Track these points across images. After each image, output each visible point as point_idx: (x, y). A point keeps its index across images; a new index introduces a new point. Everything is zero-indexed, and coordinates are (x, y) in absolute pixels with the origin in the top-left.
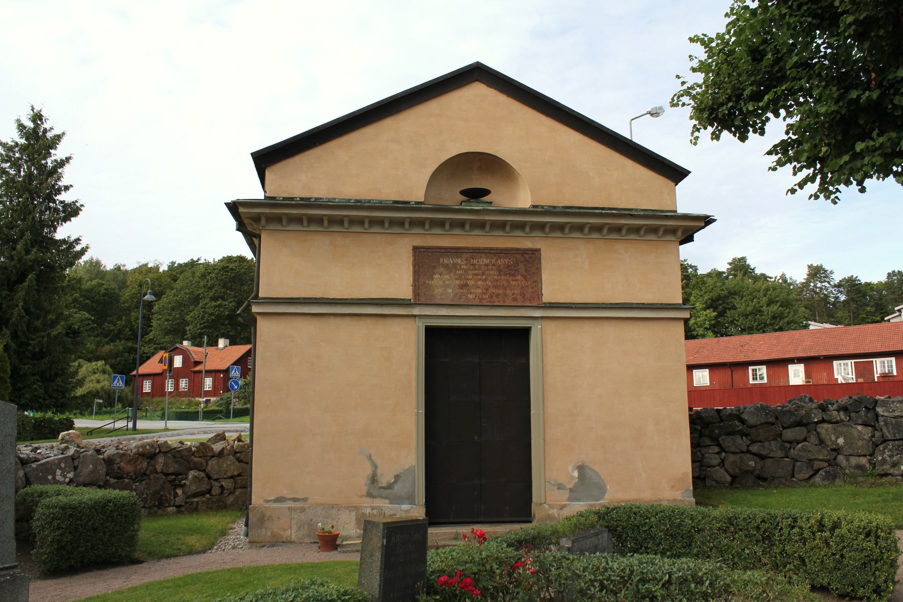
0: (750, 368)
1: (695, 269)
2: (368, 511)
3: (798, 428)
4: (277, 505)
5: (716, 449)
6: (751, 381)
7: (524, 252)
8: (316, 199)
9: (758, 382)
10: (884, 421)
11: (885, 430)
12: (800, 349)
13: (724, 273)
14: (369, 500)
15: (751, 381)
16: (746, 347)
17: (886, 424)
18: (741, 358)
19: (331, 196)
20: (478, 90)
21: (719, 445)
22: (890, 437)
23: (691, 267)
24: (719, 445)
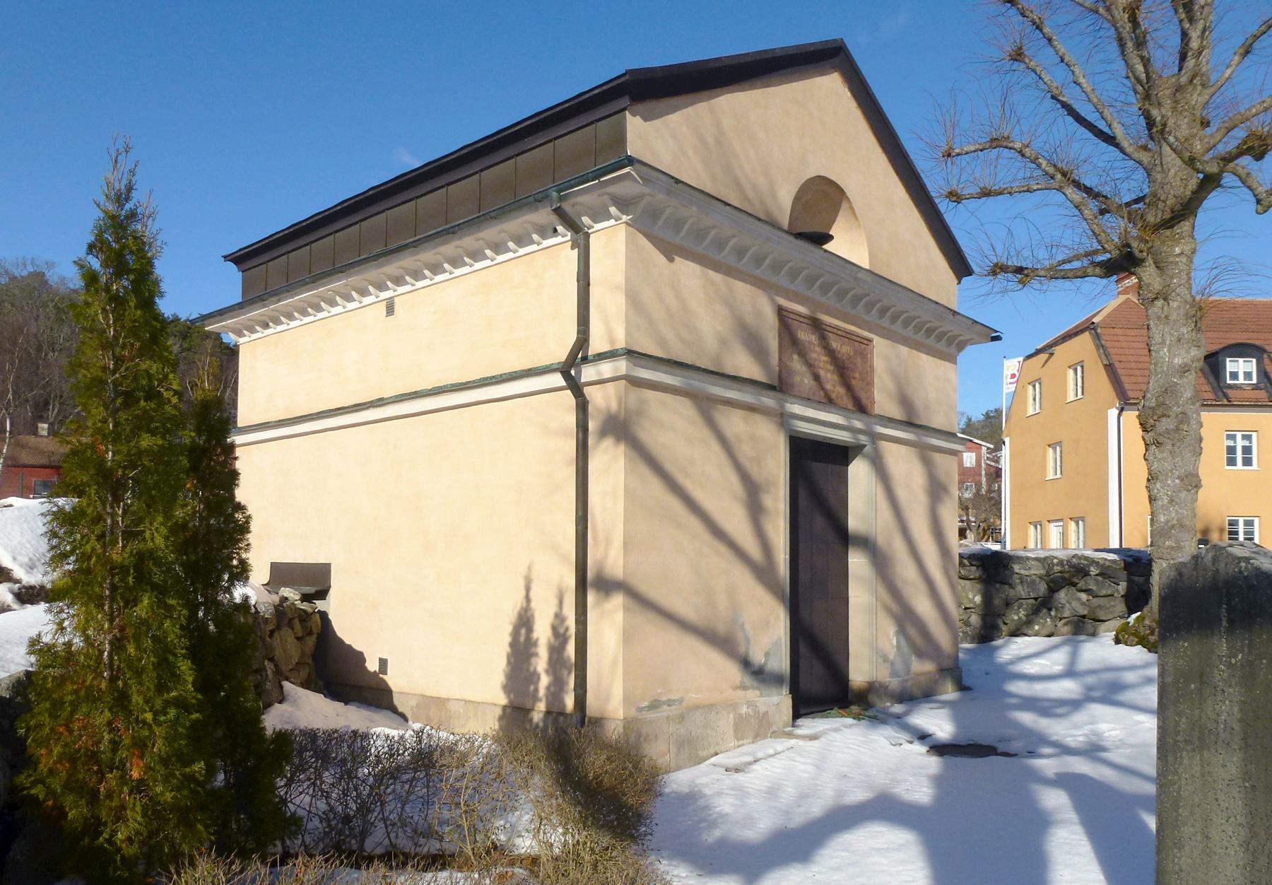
4: (652, 715)
14: (740, 693)
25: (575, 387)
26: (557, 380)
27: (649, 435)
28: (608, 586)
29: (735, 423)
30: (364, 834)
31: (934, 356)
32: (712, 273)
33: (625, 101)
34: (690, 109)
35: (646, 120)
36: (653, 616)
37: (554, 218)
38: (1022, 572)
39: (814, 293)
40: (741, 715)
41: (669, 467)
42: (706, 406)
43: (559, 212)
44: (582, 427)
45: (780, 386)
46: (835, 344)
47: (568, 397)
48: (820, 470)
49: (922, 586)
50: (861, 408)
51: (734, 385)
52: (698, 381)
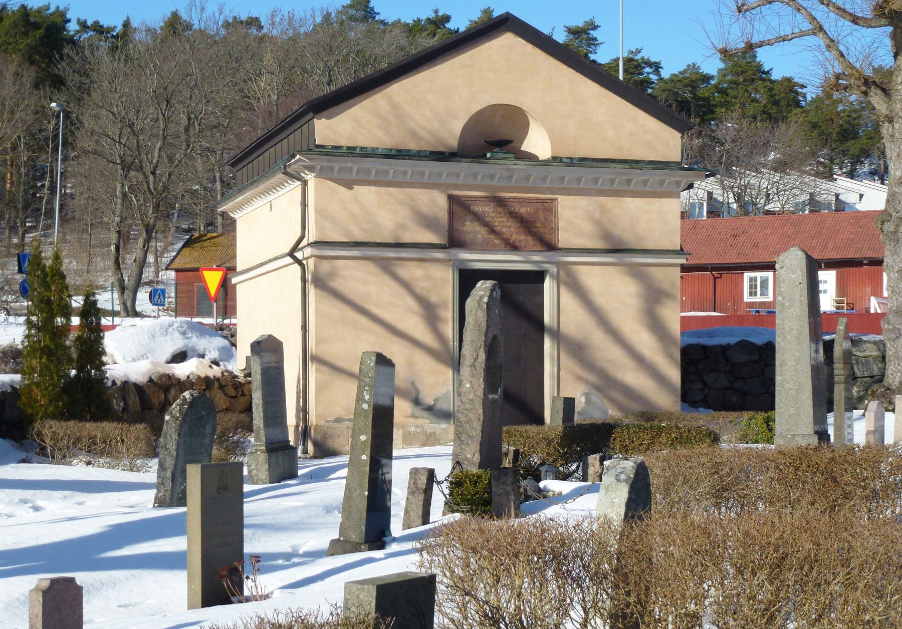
0: (747, 275)
1: (657, 67)
2: (413, 429)
3: (498, 229)
4: (336, 425)
5: (700, 386)
6: (747, 298)
7: (543, 202)
8: (362, 148)
9: (758, 299)
10: (856, 360)
11: (855, 368)
12: (831, 245)
13: (712, 77)
14: (412, 420)
15: (747, 298)
16: (742, 238)
17: (857, 363)
18: (732, 258)
19: (374, 145)
20: (508, 41)
21: (703, 381)
22: (859, 375)
23: (649, 64)
24: (703, 381)
25: (299, 262)
26: (289, 260)
27: (338, 284)
28: (320, 361)
29: (413, 272)
30: (428, 553)
31: (661, 197)
32: (391, 189)
33: (311, 115)
34: (364, 103)
35: (328, 119)
36: (343, 377)
37: (285, 177)
38: (858, 354)
39: (488, 182)
40: (409, 433)
41: (359, 301)
42: (386, 266)
43: (286, 173)
44: (304, 280)
45: (454, 242)
46: (517, 208)
47: (297, 267)
48: (521, 291)
49: (629, 363)
50: (550, 246)
51: (403, 249)
52: (384, 252)
